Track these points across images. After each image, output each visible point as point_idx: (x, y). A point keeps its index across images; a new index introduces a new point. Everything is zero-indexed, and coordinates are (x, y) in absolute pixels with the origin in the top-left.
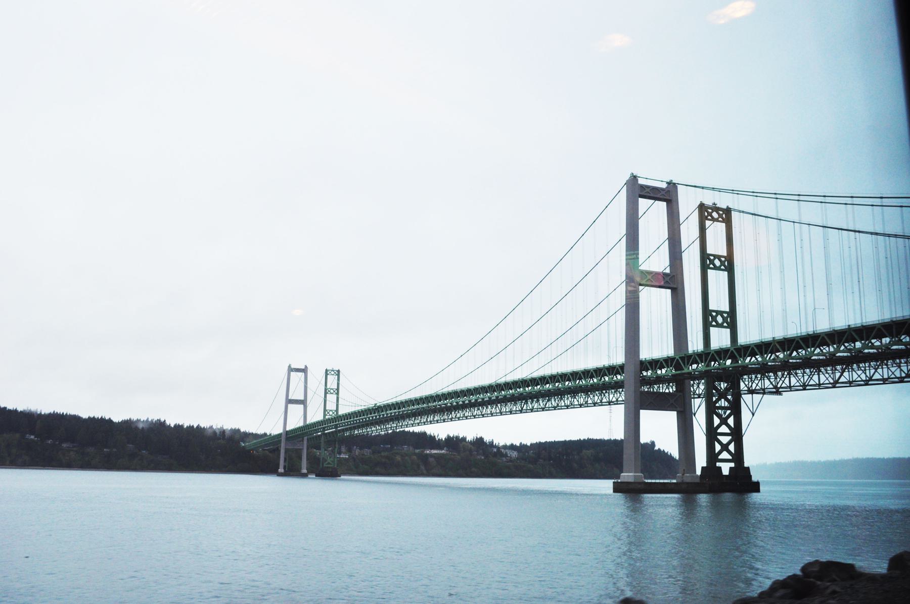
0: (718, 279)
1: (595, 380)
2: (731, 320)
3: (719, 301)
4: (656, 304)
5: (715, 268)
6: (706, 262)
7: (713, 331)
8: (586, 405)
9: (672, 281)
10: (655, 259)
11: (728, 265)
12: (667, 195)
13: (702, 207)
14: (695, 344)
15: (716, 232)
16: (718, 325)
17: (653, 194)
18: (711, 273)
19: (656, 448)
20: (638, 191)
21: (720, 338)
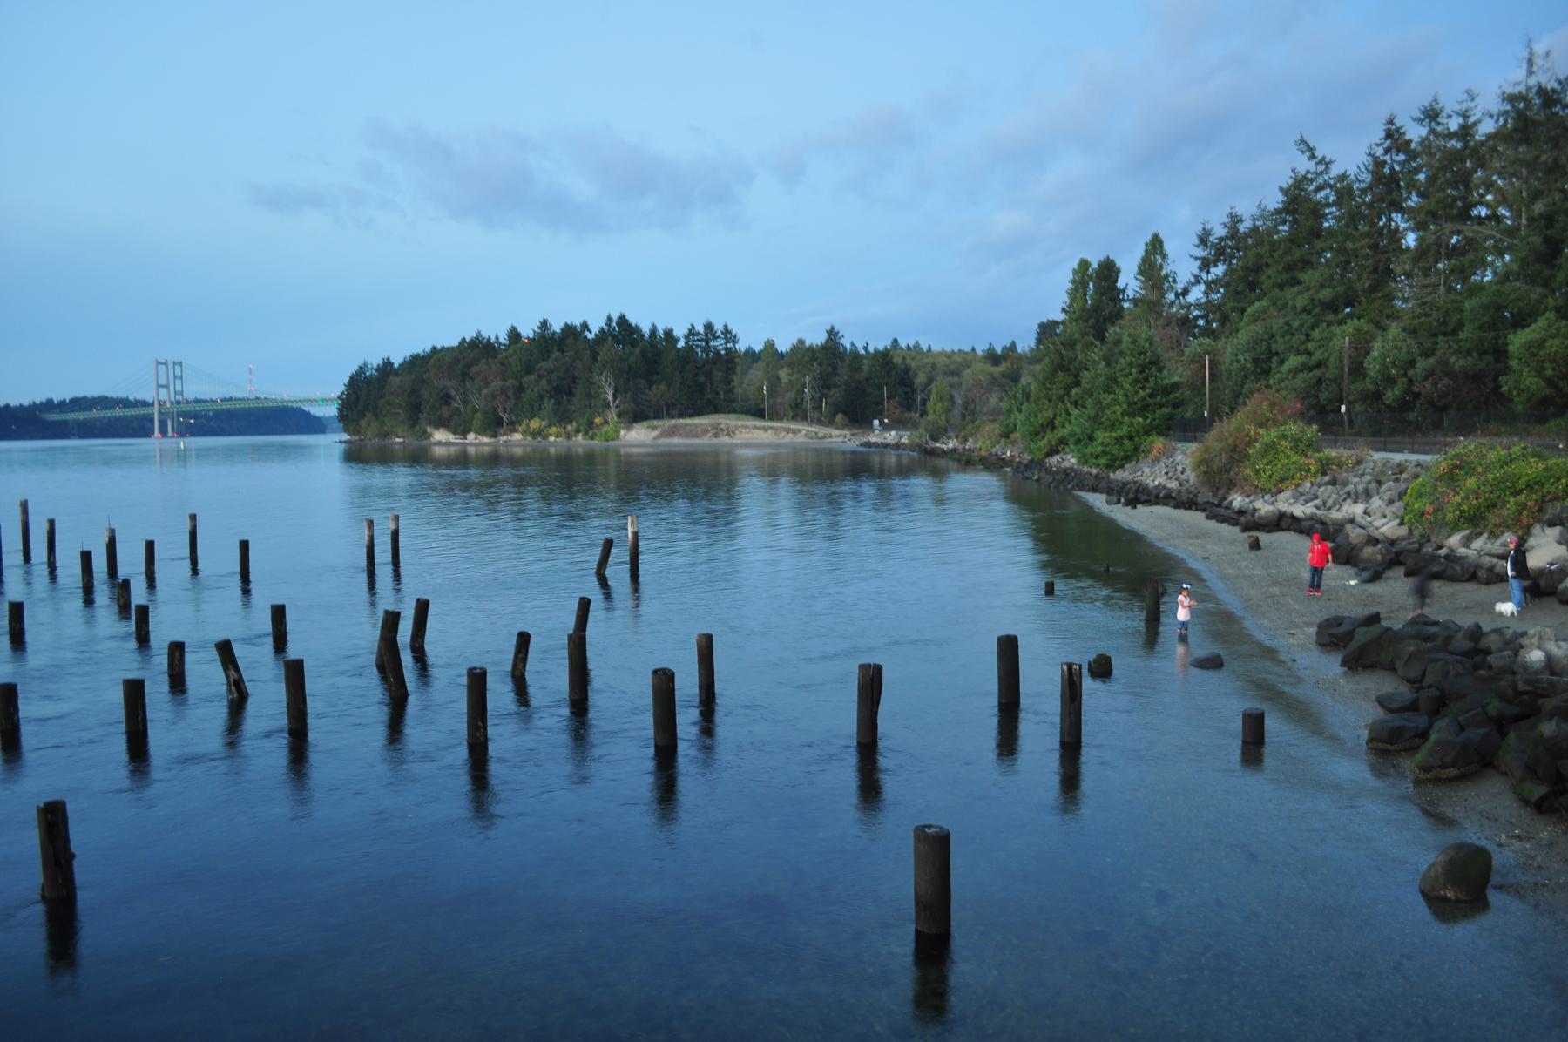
9: (167, 387)
12: (166, 364)
20: (159, 363)
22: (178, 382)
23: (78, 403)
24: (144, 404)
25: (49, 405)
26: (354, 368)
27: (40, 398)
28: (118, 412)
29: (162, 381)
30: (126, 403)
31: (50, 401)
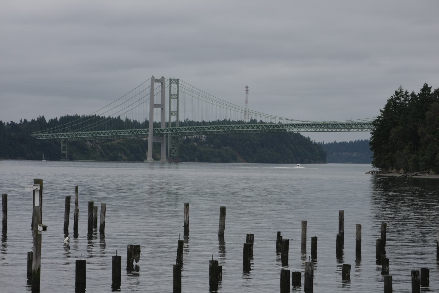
0: (174, 101)
3: (174, 109)
4: (157, 111)
6: (171, 96)
7: (172, 117)
9: (162, 106)
10: (157, 100)
11: (177, 97)
12: (162, 81)
13: (170, 79)
14: (167, 120)
15: (174, 86)
17: (157, 81)
18: (172, 100)
20: (154, 80)
21: (174, 119)
22: (174, 101)
23: (69, 122)
26: (391, 94)
28: (111, 133)
30: (115, 123)
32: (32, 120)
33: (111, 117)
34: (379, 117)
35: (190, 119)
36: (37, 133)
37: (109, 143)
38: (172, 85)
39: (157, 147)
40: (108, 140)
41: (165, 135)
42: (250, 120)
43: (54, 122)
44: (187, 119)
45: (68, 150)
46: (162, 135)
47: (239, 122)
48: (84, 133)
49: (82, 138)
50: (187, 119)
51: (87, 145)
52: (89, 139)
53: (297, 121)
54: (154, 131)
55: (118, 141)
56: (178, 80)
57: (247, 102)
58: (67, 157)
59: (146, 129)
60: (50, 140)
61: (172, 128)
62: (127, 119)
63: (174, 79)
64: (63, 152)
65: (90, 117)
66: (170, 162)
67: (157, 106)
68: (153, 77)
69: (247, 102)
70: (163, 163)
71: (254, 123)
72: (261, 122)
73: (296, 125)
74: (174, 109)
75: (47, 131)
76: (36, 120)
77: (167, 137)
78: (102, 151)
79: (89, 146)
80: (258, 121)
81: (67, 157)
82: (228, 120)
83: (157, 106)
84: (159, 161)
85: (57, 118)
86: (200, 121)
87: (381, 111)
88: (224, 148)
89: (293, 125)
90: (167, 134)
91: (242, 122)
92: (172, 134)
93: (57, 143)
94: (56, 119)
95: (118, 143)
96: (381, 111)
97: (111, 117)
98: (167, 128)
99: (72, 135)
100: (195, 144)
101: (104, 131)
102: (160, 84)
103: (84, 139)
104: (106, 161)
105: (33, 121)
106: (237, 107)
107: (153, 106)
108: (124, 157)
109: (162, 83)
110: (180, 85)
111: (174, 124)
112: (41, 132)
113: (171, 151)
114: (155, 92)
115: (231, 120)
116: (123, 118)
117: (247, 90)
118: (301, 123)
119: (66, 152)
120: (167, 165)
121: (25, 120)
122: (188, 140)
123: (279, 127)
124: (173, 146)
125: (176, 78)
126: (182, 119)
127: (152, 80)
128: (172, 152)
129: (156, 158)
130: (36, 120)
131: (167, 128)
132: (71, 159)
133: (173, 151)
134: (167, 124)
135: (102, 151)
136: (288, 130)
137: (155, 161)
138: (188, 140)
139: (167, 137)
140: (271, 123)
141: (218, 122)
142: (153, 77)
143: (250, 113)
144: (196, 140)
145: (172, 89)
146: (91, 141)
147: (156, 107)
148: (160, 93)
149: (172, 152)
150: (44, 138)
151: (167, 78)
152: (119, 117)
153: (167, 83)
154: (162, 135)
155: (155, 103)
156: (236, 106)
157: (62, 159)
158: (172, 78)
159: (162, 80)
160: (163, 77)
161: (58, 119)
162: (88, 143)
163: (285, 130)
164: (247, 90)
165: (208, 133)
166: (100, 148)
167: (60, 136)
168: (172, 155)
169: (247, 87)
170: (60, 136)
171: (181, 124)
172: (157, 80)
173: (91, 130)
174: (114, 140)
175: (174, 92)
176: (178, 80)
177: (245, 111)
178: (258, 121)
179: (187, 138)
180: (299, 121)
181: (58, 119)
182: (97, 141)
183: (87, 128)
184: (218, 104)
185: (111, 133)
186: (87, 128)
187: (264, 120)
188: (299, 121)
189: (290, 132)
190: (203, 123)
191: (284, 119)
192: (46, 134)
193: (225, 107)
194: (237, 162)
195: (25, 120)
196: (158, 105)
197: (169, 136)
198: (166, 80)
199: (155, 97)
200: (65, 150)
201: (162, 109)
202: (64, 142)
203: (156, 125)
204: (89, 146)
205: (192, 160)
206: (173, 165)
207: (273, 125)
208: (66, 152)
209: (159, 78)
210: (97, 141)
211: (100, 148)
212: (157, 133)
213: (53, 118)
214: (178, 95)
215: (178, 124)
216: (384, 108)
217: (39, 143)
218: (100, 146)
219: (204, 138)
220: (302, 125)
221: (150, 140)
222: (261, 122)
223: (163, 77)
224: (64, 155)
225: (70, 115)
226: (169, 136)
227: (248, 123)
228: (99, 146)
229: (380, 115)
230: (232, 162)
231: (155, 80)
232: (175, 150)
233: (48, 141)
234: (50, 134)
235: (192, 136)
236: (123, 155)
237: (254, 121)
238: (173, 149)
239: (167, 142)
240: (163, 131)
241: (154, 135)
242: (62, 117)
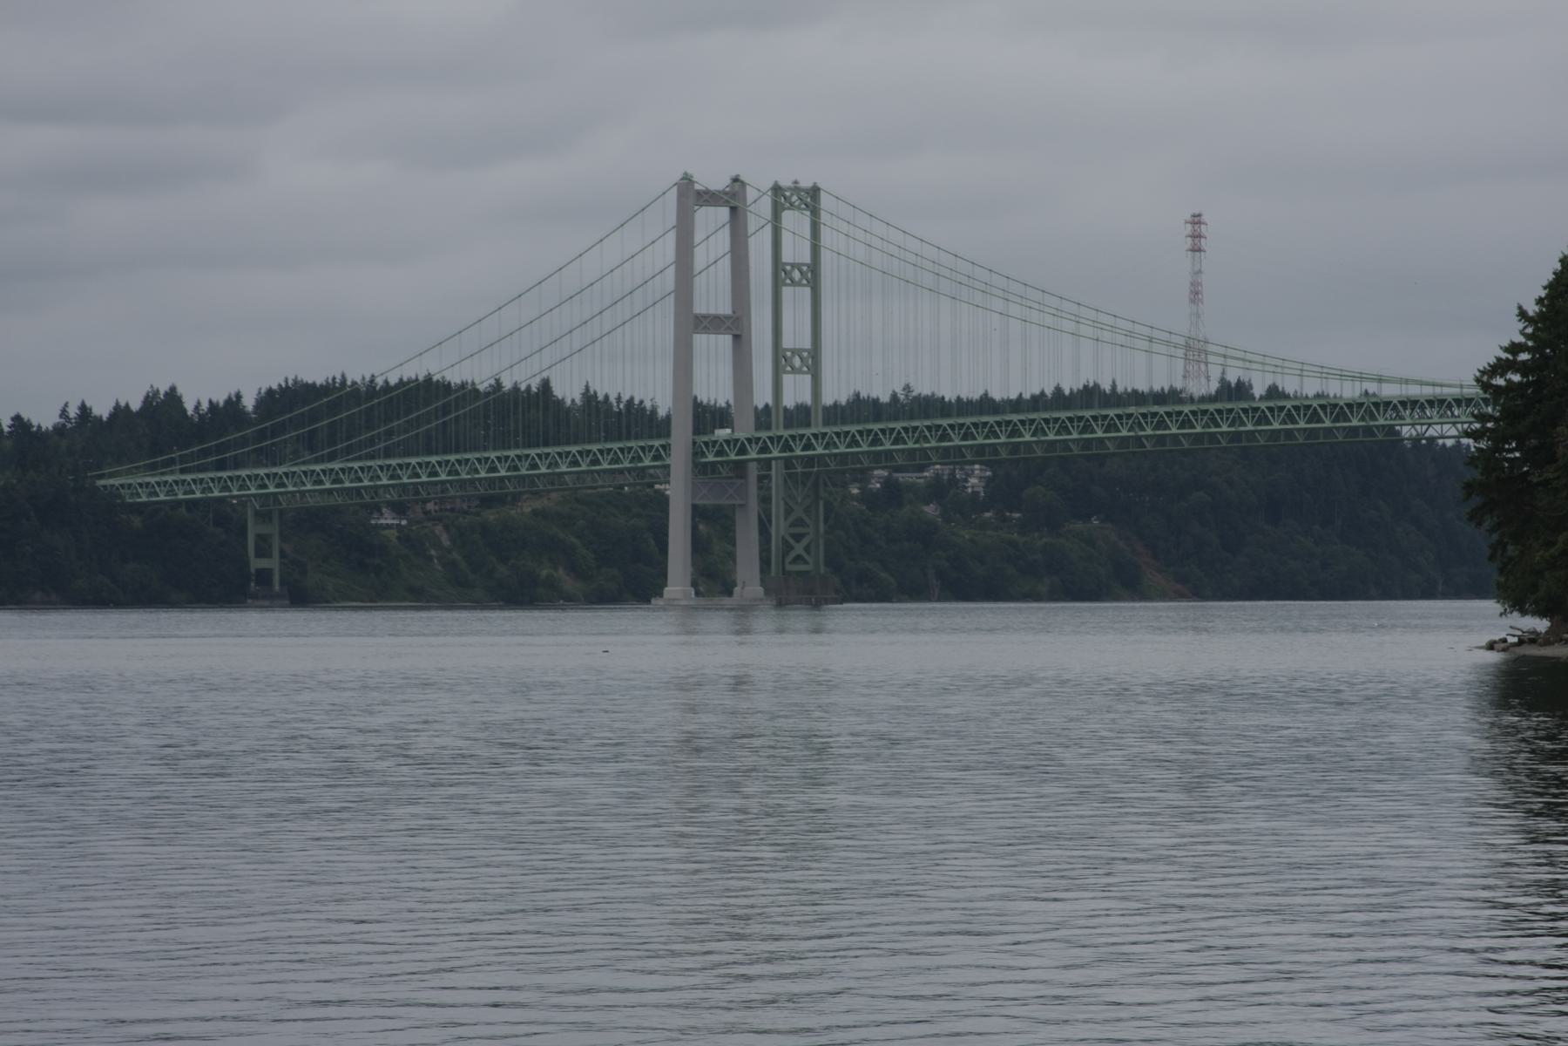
0: (796, 301)
1: (1490, 409)
2: (813, 362)
3: (796, 334)
4: (713, 351)
5: (793, 283)
6: (780, 273)
7: (788, 380)
8: (1325, 373)
9: (735, 326)
10: (713, 296)
11: (812, 275)
12: (732, 198)
13: (777, 189)
14: (762, 396)
15: (795, 222)
16: (794, 371)
17: (709, 198)
18: (787, 292)
19: (1067, 392)
20: (691, 196)
21: (796, 391)
22: (796, 301)
23: (306, 416)
24: (635, 421)
25: (160, 426)
27: (114, 389)
28: (486, 464)
29: (713, 296)
30: (527, 414)
31: (163, 407)
32: (986, 394)
33: (380, 381)
34: (1514, 348)
35: (923, 388)
36: (129, 472)
37: (490, 516)
38: (788, 217)
39: (713, 526)
40: (487, 502)
41: (753, 471)
42: (1214, 386)
43: (227, 413)
44: (907, 388)
45: (283, 554)
46: (739, 468)
47: (1160, 398)
48: (356, 465)
49: (463, 484)
50: (907, 388)
51: (377, 526)
52: (393, 496)
53: (1407, 382)
54: (697, 452)
55: (537, 504)
56: (815, 192)
57: (1196, 294)
58: (277, 588)
59: (657, 443)
60: (193, 505)
61: (786, 433)
62: (589, 397)
63: (796, 189)
64: (256, 564)
65: (326, 389)
66: (781, 604)
67: (711, 323)
68: (687, 180)
69: (1196, 294)
70: (745, 609)
71: (1239, 399)
72: (1273, 392)
73: (1403, 403)
74: (796, 334)
75: (172, 462)
76: (135, 406)
77: (763, 479)
78: (455, 555)
79: (392, 534)
80: (1259, 390)
81: (277, 588)
82: (1107, 387)
83: (711, 323)
84: (727, 601)
85: (239, 396)
86: (972, 392)
87: (1522, 314)
88: (1079, 526)
89: (1412, 404)
90: (766, 464)
91: (1172, 396)
92: (788, 463)
93: (224, 516)
94: (234, 403)
95: (535, 513)
96: (1522, 314)
97: (380, 381)
98: (764, 435)
99: (306, 479)
100: (931, 510)
101: (452, 458)
102: (723, 213)
103: (417, 493)
104: (480, 604)
105: (120, 412)
106: (1109, 320)
107: (693, 323)
108: (569, 583)
109: (733, 210)
110: (824, 217)
111: (801, 415)
112: (152, 468)
113: (787, 548)
114: (700, 258)
115: (1027, 396)
116: (568, 390)
117: (1197, 236)
118: (1428, 391)
119: (273, 563)
120: (765, 620)
121: (84, 410)
122: (893, 492)
123: (1315, 417)
124: (792, 525)
125: (806, 183)
126: (836, 392)
127: (682, 195)
128: (792, 555)
129: (713, 579)
130: (135, 406)
131: (764, 435)
132: (300, 596)
133: (799, 549)
134: (763, 417)
135: (455, 555)
136: (1406, 431)
137: (702, 601)
138: (893, 492)
139: (763, 479)
140: (1318, 396)
141: (1060, 399)
142: (687, 180)
143: (1211, 358)
144: (937, 491)
145: (786, 238)
146: (399, 509)
147: (706, 330)
148: (727, 261)
149: (792, 555)
150: (162, 497)
151: (759, 182)
152: (546, 385)
153: (759, 208)
154: (739, 468)
155: (700, 308)
156: (1103, 318)
157: (255, 597)
158: (785, 182)
159: (734, 195)
160: (736, 180)
161: (249, 403)
162: (388, 519)
163: (1390, 431)
164: (1197, 236)
165: (1149, 447)
166: (446, 542)
167: (248, 483)
168: (789, 567)
169: (1197, 220)
170: (248, 483)
171: (835, 414)
172: (707, 192)
173: (388, 453)
174: (516, 498)
175: (796, 250)
176: (815, 192)
177: (1188, 347)
178: (1259, 390)
179: (889, 484)
180: (1422, 383)
181: (249, 403)
182: (430, 506)
183: (371, 441)
184: (1014, 310)
185: (486, 464)
186: (371, 441)
187: (1289, 385)
188: (1422, 383)
189: (1416, 440)
190: (986, 404)
191: (1342, 376)
192: (170, 478)
193: (1069, 326)
194: (1144, 596)
195: (84, 410)
196: (717, 317)
197: (776, 471)
198: (751, 194)
199: (700, 283)
200: (270, 556)
201: (737, 338)
202: (263, 516)
203: (707, 417)
204: (392, 534)
205: (910, 589)
206: (799, 618)
207: (1288, 404)
208: (273, 563)
209: (719, 183)
210: (430, 506)
211: (446, 542)
212: (711, 458)
213: (220, 398)
214: (815, 267)
215: (778, 419)
216: (1540, 301)
217: (137, 521)
218: (446, 528)
219: (975, 480)
220: (1431, 403)
221: (678, 493)
222: (1273, 392)
223: (736, 180)
224: (264, 577)
225: (309, 378)
226: (776, 471)
227: (1203, 399)
228: (439, 529)
229: (1520, 339)
230: (1117, 598)
231: (699, 193)
232: (805, 541)
233: (183, 510)
234: (188, 477)
235: (921, 468)
236: (561, 573)
237: (1240, 391)
238: (798, 538)
239: (765, 500)
240: (742, 451)
241: (701, 470)
242: (270, 391)
